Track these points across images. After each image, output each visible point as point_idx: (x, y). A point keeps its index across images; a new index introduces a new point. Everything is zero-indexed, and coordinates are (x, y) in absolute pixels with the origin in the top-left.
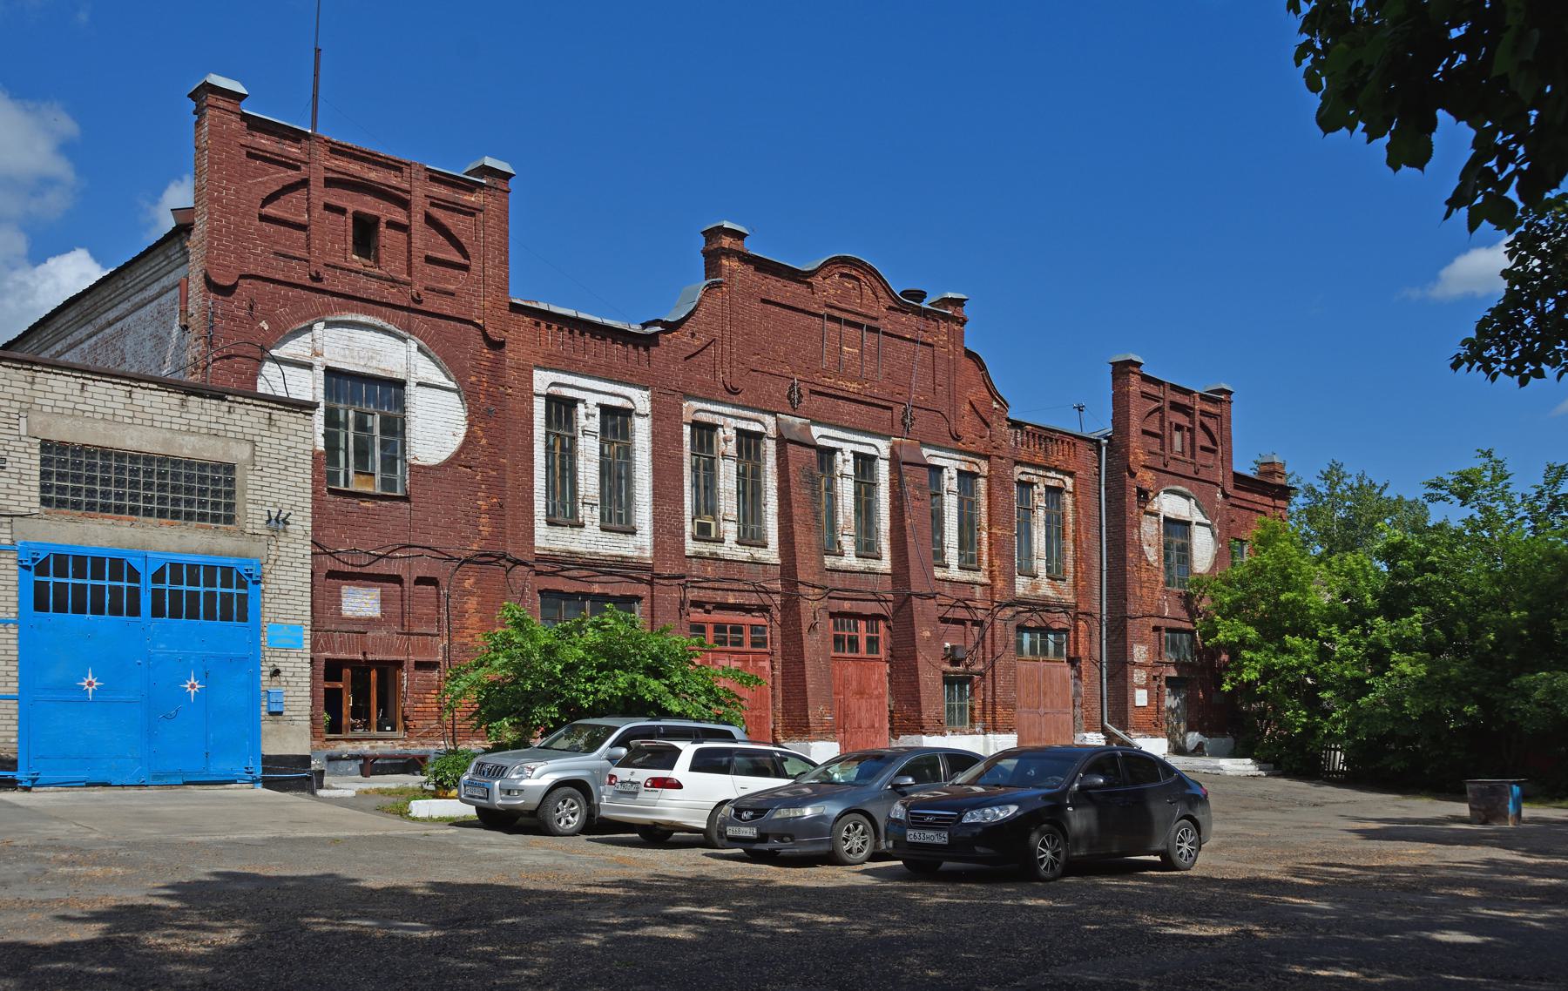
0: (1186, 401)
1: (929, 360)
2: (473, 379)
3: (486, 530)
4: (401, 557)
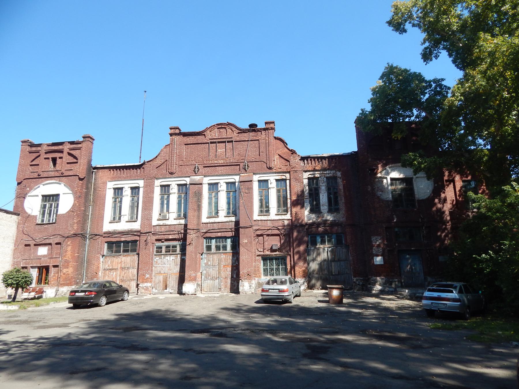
1: (257, 146)
3: (75, 228)
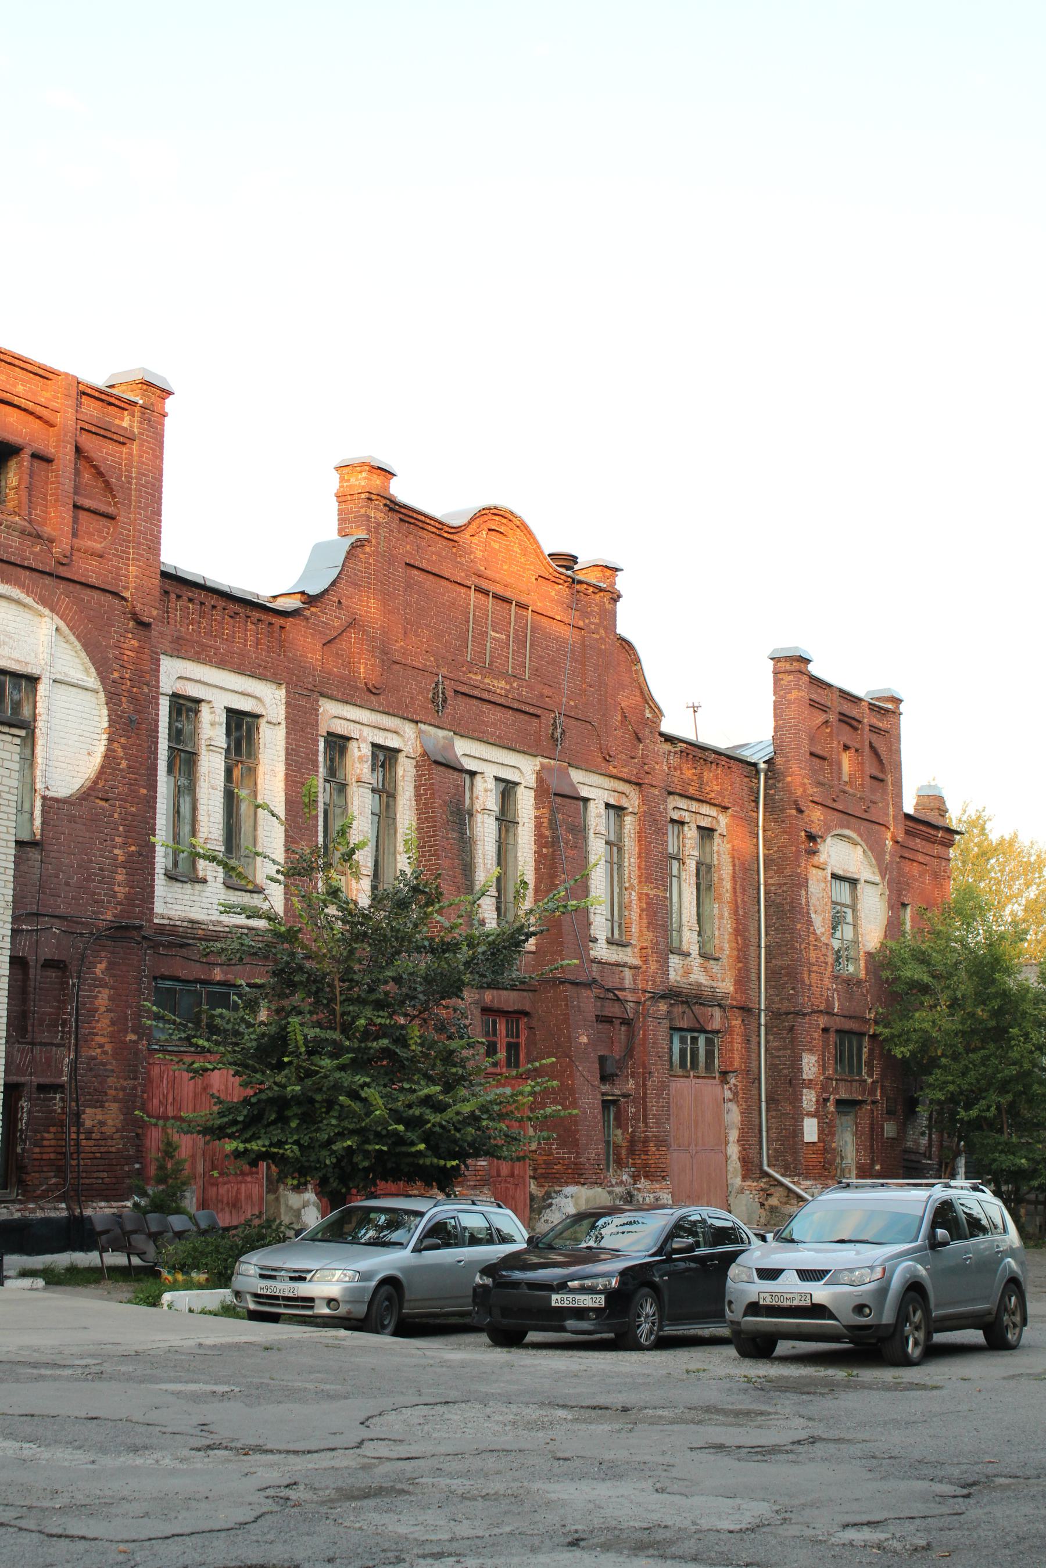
0: (854, 712)
2: (116, 675)
4: (27, 931)
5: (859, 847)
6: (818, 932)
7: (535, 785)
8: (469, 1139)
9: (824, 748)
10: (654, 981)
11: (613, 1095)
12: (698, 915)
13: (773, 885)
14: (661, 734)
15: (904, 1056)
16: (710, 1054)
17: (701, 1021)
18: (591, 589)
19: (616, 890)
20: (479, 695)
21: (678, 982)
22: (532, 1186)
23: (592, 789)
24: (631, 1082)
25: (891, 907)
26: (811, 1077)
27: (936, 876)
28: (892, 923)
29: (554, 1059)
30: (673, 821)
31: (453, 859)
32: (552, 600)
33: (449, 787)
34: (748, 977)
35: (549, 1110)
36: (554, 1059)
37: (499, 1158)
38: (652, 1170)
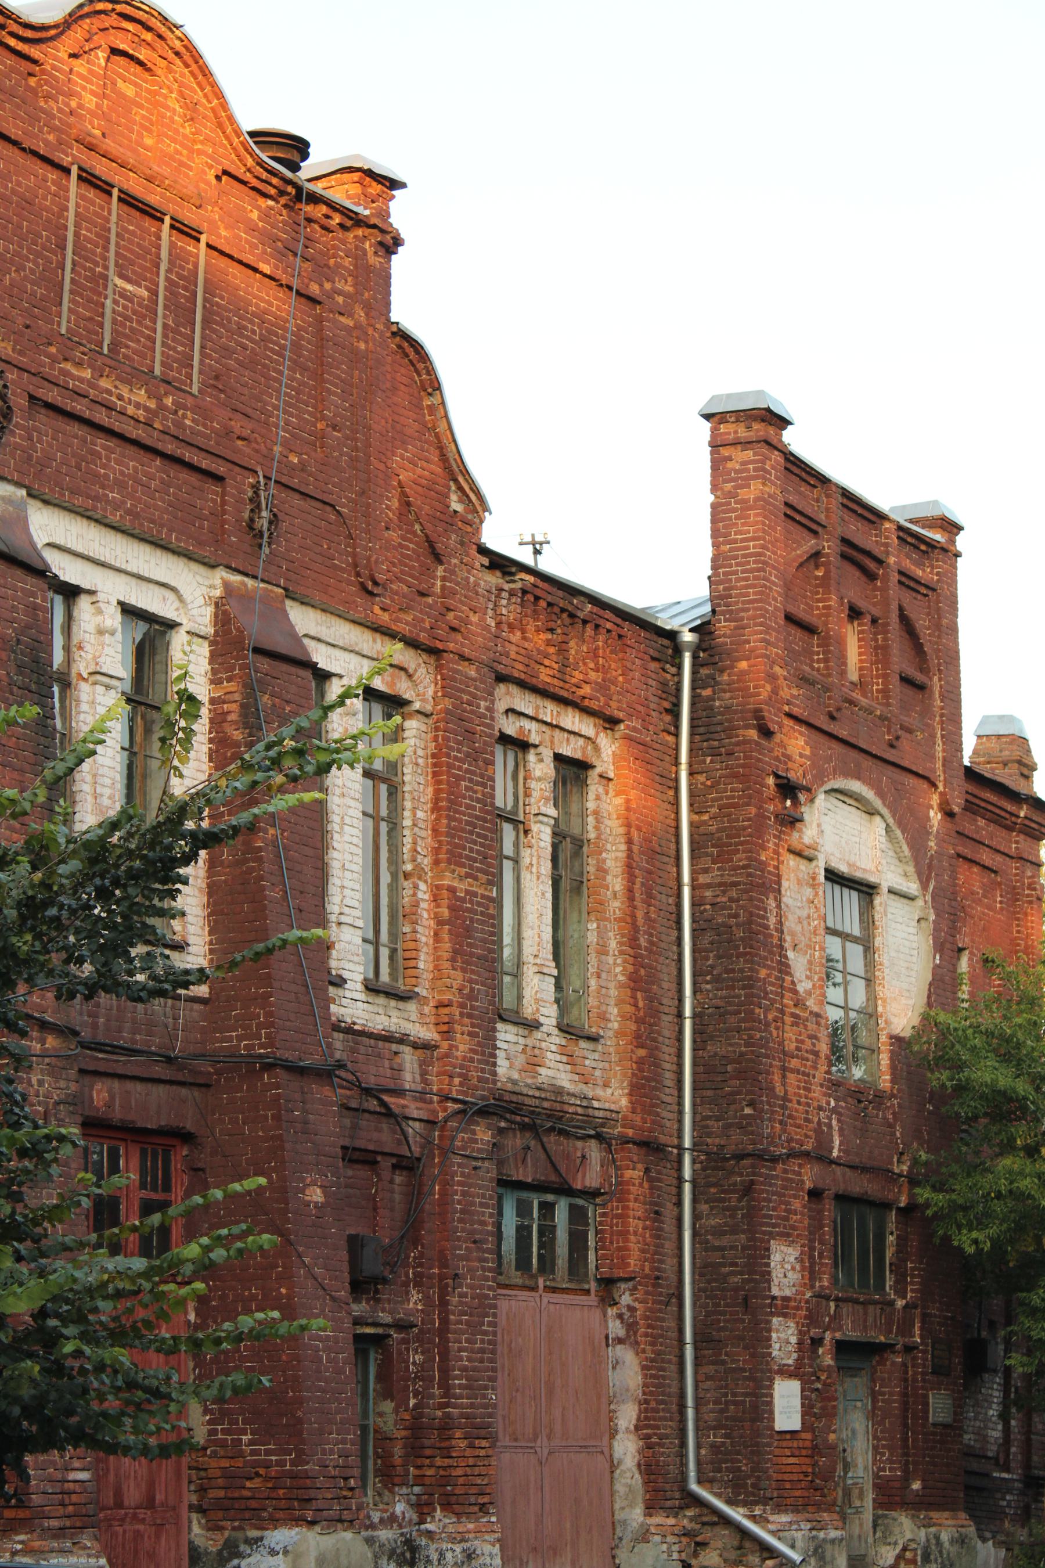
5: (877, 819)
6: (800, 988)
7: (210, 630)
8: (26, 1392)
9: (811, 608)
10: (465, 1077)
11: (375, 1324)
12: (556, 944)
13: (708, 886)
14: (484, 551)
15: (979, 1251)
16: (578, 1242)
17: (563, 1169)
18: (337, 219)
19: (385, 878)
20: (87, 414)
21: (515, 1082)
22: (196, 1529)
23: (337, 652)
24: (415, 1296)
25: (939, 947)
26: (788, 1293)
27: (1014, 896)
28: (942, 981)
29: (262, 1181)
30: (505, 739)
31: (21, 771)
32: (253, 229)
33: (14, 609)
34: (657, 1078)
35: (246, 1322)
36: (262, 1181)
37: (112, 1448)
38: (459, 1490)
